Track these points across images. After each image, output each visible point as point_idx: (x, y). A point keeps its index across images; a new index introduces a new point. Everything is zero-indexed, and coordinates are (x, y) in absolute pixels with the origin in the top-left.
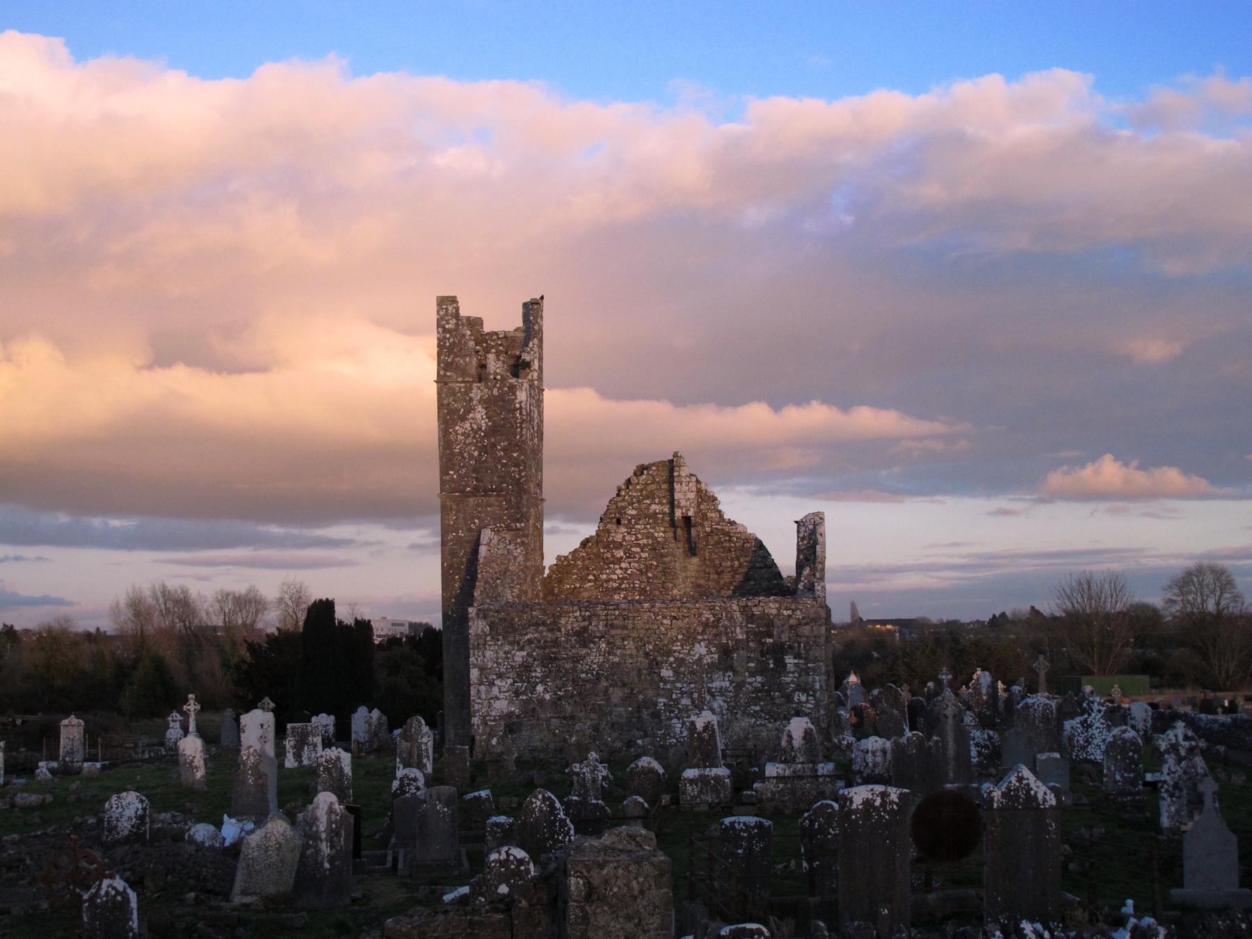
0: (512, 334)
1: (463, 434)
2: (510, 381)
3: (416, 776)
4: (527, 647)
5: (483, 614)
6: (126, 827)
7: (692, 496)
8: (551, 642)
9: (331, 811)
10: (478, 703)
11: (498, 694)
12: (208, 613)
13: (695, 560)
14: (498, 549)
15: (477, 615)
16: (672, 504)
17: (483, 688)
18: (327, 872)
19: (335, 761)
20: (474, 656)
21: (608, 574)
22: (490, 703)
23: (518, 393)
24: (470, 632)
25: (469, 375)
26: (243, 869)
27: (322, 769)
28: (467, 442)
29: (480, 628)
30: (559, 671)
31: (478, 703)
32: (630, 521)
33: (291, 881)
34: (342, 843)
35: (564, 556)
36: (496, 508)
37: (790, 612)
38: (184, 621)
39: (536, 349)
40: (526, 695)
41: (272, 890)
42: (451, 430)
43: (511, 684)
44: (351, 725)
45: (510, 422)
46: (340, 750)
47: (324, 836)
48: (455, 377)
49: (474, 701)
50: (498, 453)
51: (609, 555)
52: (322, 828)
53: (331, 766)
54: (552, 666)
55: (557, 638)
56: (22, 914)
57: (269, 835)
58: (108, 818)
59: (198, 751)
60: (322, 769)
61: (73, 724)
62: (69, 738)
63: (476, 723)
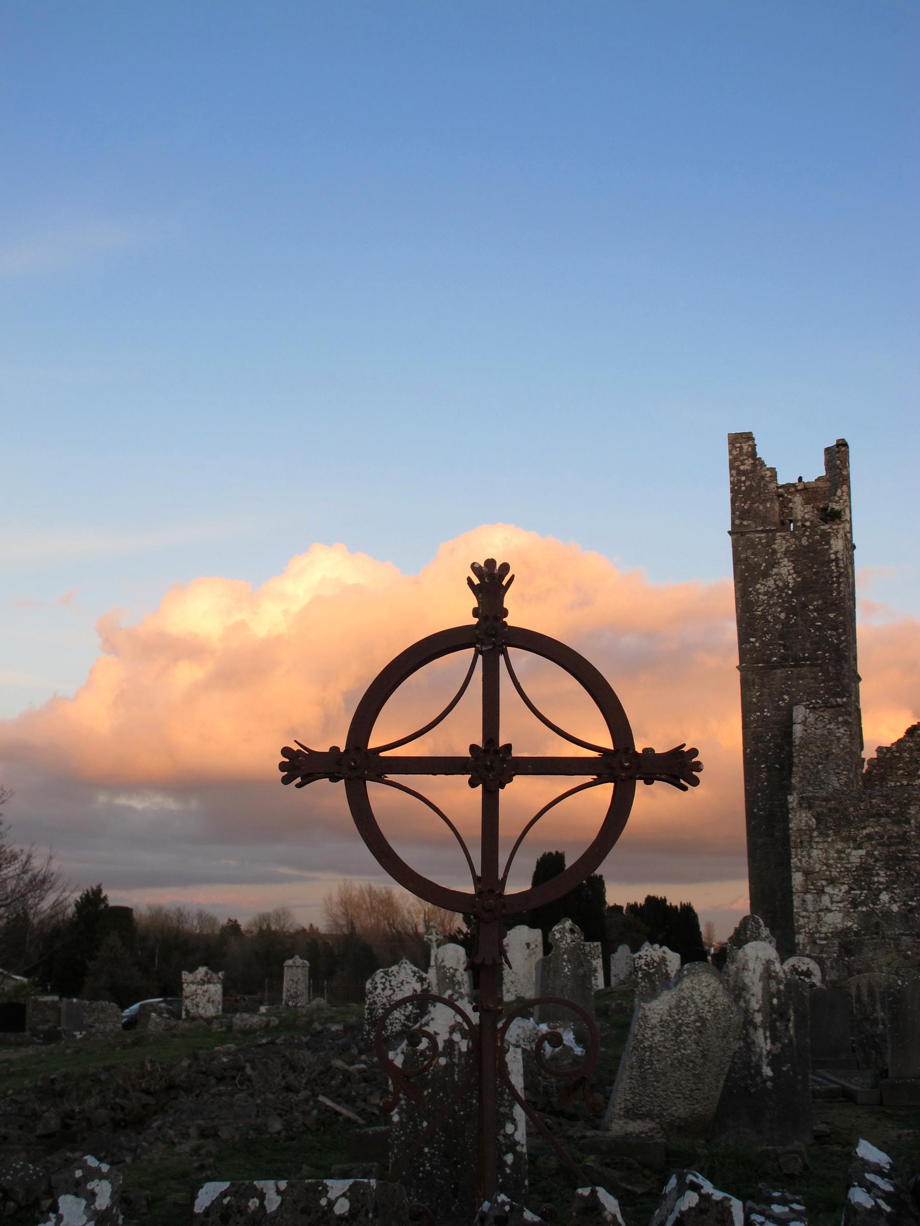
0: (813, 485)
1: (765, 594)
2: (823, 527)
3: (808, 969)
4: (866, 844)
5: (807, 803)
6: (396, 1018)
8: (899, 838)
9: (768, 975)
10: (804, 917)
11: (829, 905)
12: (409, 912)
14: (815, 729)
15: (800, 804)
17: (809, 897)
18: (769, 1084)
19: (659, 964)
20: (796, 856)
22: (819, 916)
23: (832, 542)
24: (791, 825)
26: (632, 1068)
27: (640, 975)
28: (771, 602)
29: (803, 821)
30: (909, 874)
31: (804, 917)
33: (717, 1094)
34: (792, 1032)
35: (886, 748)
36: (810, 681)
38: (388, 919)
40: (867, 906)
41: (681, 1109)
42: (750, 589)
43: (845, 892)
44: (610, 966)
45: (824, 577)
46: (665, 948)
47: (758, 1018)
48: (754, 527)
49: (798, 913)
50: (810, 613)
52: (755, 1005)
53: (652, 971)
54: (900, 869)
55: (905, 832)
56: (237, 1138)
57: (684, 1003)
58: (370, 1004)
59: (462, 962)
60: (640, 975)
61: (297, 964)
62: (293, 981)
63: (801, 942)
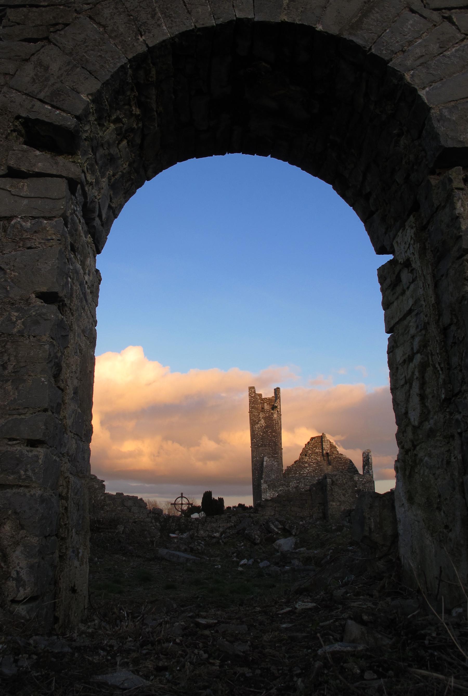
5: (266, 482)
7: (329, 446)
13: (330, 466)
15: (264, 482)
16: (322, 449)
21: (303, 472)
25: (259, 410)
32: (309, 455)
37: (362, 479)
39: (279, 402)
51: (303, 466)
